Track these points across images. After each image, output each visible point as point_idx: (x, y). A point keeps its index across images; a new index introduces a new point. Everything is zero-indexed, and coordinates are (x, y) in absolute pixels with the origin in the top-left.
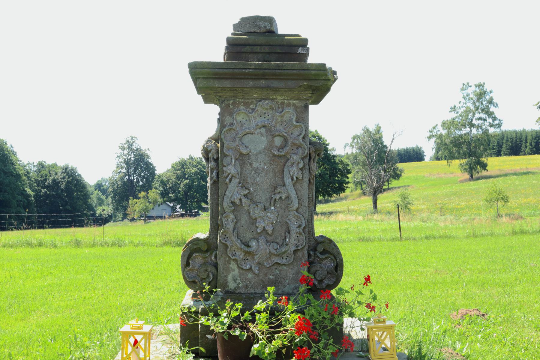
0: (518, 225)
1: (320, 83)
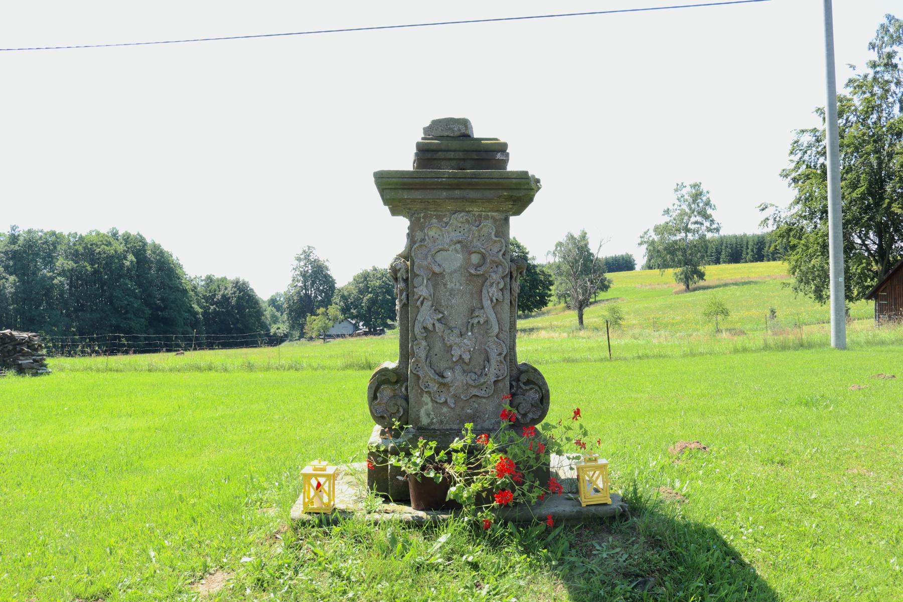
0: (739, 341)
1: (521, 193)
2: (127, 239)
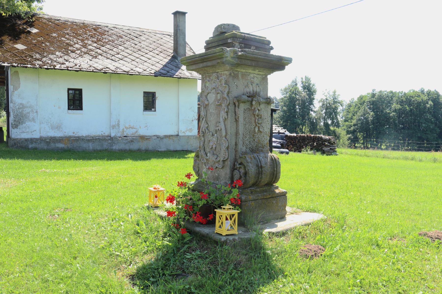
2: (429, 93)
